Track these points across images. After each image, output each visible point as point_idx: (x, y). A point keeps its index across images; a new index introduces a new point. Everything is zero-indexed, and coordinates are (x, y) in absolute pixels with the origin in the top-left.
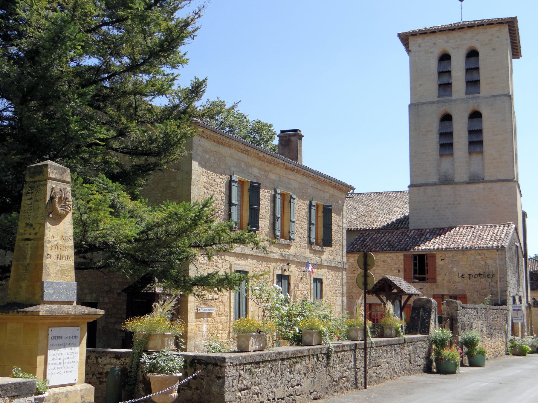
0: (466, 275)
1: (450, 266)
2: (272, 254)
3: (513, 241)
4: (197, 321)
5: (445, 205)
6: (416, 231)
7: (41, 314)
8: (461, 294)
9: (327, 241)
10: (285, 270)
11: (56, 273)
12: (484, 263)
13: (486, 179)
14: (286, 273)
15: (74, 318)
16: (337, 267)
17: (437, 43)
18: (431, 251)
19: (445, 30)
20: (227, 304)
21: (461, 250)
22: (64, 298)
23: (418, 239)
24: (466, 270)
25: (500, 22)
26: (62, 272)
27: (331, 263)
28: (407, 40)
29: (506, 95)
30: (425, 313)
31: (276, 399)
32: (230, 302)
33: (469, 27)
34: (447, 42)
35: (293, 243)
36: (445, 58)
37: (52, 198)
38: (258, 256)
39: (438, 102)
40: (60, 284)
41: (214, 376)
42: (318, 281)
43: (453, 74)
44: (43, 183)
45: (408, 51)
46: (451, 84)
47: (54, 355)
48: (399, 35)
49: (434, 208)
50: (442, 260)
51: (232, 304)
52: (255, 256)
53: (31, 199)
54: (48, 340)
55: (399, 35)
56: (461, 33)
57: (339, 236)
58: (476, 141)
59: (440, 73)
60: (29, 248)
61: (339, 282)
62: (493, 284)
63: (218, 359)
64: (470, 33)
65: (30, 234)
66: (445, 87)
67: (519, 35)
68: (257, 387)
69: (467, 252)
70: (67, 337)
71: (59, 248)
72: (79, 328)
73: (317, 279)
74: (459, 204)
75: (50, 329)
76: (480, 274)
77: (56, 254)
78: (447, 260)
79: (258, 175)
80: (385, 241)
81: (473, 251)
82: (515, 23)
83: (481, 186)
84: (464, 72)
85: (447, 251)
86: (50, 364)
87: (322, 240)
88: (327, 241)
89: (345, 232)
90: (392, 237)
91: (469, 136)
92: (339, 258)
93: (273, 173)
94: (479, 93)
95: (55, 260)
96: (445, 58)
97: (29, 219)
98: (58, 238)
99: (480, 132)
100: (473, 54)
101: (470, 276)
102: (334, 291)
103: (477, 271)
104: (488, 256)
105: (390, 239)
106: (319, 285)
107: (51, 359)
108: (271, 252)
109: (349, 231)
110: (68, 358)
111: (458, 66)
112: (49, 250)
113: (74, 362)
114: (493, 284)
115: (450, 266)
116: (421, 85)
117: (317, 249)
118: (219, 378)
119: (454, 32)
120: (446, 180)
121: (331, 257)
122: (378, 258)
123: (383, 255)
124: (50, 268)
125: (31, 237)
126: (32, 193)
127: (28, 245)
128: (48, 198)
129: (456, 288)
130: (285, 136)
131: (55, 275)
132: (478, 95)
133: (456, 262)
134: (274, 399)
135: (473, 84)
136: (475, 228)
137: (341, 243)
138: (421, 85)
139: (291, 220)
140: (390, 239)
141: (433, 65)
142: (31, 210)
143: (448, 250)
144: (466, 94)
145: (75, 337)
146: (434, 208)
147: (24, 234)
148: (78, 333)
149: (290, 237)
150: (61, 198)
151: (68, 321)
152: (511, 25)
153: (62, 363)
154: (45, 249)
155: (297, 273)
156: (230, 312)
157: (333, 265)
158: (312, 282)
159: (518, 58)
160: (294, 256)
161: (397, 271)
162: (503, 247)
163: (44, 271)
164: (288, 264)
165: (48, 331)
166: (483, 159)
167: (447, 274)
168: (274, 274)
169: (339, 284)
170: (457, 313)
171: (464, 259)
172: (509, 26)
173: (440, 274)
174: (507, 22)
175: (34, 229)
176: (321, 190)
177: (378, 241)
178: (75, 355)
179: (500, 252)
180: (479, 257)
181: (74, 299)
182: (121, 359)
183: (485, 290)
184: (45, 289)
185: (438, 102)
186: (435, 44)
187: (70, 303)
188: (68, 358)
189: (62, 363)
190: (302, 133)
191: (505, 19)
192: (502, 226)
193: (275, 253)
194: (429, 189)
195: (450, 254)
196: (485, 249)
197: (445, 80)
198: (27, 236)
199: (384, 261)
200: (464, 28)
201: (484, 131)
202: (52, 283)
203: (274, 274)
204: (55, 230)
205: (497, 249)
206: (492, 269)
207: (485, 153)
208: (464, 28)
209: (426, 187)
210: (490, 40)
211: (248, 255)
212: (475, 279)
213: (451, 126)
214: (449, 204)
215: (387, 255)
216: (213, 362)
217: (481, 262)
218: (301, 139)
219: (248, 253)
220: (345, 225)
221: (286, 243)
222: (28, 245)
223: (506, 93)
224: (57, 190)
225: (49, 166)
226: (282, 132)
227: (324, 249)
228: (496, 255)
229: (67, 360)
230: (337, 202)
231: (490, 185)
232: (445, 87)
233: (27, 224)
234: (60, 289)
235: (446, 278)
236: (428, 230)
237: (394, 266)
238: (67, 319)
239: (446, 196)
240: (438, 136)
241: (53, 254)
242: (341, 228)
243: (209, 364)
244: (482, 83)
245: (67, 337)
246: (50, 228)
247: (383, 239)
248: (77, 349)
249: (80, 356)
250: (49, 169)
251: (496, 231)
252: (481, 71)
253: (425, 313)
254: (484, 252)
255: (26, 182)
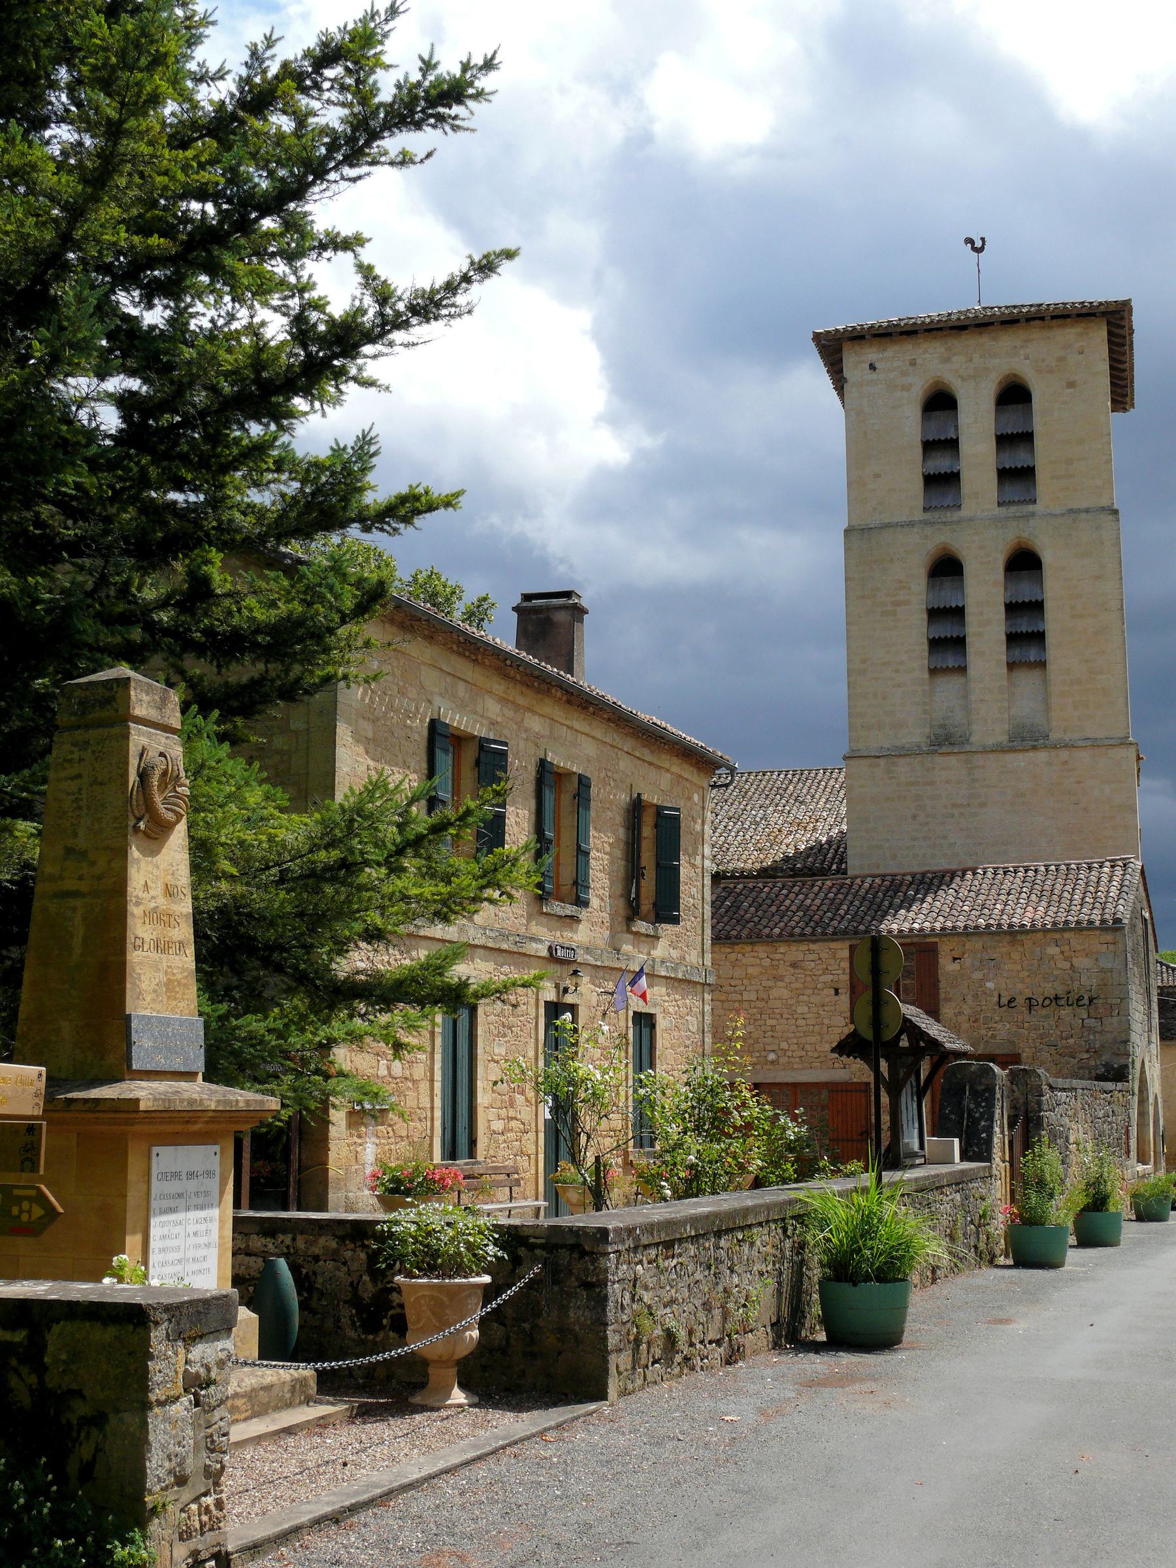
0: (1020, 1000)
1: (977, 975)
2: (534, 945)
3: (1138, 906)
4: (351, 1135)
5: (945, 806)
6: (878, 881)
7: (142, 1107)
8: (1006, 1051)
9: (666, 909)
10: (566, 990)
11: (155, 991)
12: (1067, 965)
13: (1054, 736)
14: (569, 999)
15: (212, 1120)
16: (689, 982)
17: (919, 361)
18: (925, 936)
19: (940, 329)
20: (424, 1086)
21: (1005, 933)
22: (178, 1064)
23: (886, 903)
24: (1020, 986)
25: (1084, 314)
26: (170, 986)
27: (675, 969)
28: (839, 350)
29: (1103, 509)
30: (978, 1105)
31: (706, 1342)
32: (432, 1081)
33: (1004, 323)
34: (947, 360)
35: (584, 914)
36: (940, 402)
37: (143, 776)
38: (499, 950)
39: (926, 523)
40: (167, 1022)
41: (573, 1282)
42: (645, 1022)
43: (965, 447)
44: (116, 730)
45: (839, 383)
46: (958, 474)
47: (163, 1225)
48: (817, 337)
49: (914, 817)
50: (955, 959)
51: (438, 1086)
52: (491, 949)
53: (79, 776)
54: (149, 1182)
55: (817, 337)
56: (984, 340)
57: (695, 892)
58: (1026, 636)
59: (929, 447)
60: (78, 919)
61: (693, 1023)
62: (1091, 1022)
63: (586, 1233)
64: (1007, 341)
65: (81, 878)
66: (942, 484)
67: (1131, 348)
68: (668, 1310)
69: (1023, 937)
70: (191, 1175)
71: (159, 920)
72: (217, 1148)
73: (641, 1014)
74: (982, 805)
75: (155, 1150)
76: (1057, 998)
77: (154, 937)
78: (967, 961)
79: (499, 719)
80: (794, 908)
81: (1040, 935)
82: (1126, 314)
83: (1042, 756)
84: (992, 443)
85: (968, 934)
86: (157, 1251)
87: (654, 905)
88: (666, 909)
89: (708, 881)
90: (812, 896)
91: (1006, 619)
92: (693, 957)
93: (534, 712)
94: (1035, 502)
95: (154, 956)
96: (940, 402)
97: (75, 835)
98: (157, 890)
99: (1037, 607)
100: (1014, 395)
101: (1030, 1003)
102: (682, 1049)
103: (1049, 989)
104: (1079, 948)
105: (808, 902)
106: (646, 1031)
107: (157, 1238)
108: (532, 939)
109: (717, 878)
110: (195, 1234)
111: (977, 424)
112: (139, 929)
113: (208, 1245)
114: (1091, 1022)
115: (977, 975)
116: (877, 476)
117: (643, 931)
118: (588, 1286)
119: (965, 335)
120: (945, 740)
121: (675, 954)
122: (778, 956)
123: (793, 948)
124: (143, 977)
125: (84, 887)
126: (81, 760)
127: (74, 909)
128: (133, 777)
129: (993, 1036)
130: (537, 610)
131: (153, 995)
132: (1031, 508)
133: (993, 963)
134: (702, 1342)
135: (1017, 477)
136: (1036, 871)
137: (698, 913)
138: (877, 476)
139: (579, 846)
140: (808, 902)
141: (910, 424)
142: (80, 808)
143: (971, 933)
144: (999, 504)
145: (209, 1174)
146: (914, 817)
147: (61, 878)
148: (214, 1163)
149: (578, 897)
150: (165, 773)
151: (197, 1127)
152: (1114, 319)
153: (182, 1248)
154: (130, 921)
155: (594, 999)
156: (432, 1108)
157: (680, 976)
158: (630, 1024)
159: (1125, 410)
160: (588, 950)
161: (833, 991)
162: (1117, 921)
163: (128, 986)
164: (575, 973)
165: (149, 1158)
166: (1045, 682)
167: (969, 998)
168: (537, 1000)
169: (694, 1029)
170: (1039, 1103)
171: (1016, 956)
172: (1109, 323)
173: (948, 1000)
174: (1104, 314)
175: (93, 864)
176: (651, 764)
177: (774, 909)
178: (210, 1226)
179: (1109, 937)
180: (1053, 950)
181: (199, 1065)
182: (281, 1237)
183: (1071, 1041)
184: (134, 1037)
185: (926, 523)
186: (913, 363)
187: (189, 1076)
188: (195, 1234)
189: (182, 1248)
190: (584, 603)
191: (1101, 304)
192: (1108, 864)
193: (541, 941)
194: (902, 767)
195: (976, 944)
196: (1071, 929)
197: (941, 463)
198: (69, 885)
199: (794, 965)
200: (992, 324)
201: (1048, 606)
202: (150, 1018)
203: (537, 1000)
204: (150, 868)
205: (1104, 927)
206: (1089, 982)
207: (972, 671)
208: (992, 324)
209: (896, 760)
210: (1061, 359)
211: (476, 946)
212: (1044, 1012)
213: (961, 587)
214: (954, 805)
215: (803, 947)
216: (571, 1240)
217: (1059, 965)
218: (581, 621)
219: (476, 942)
220: (707, 863)
221: (569, 913)
222: (74, 909)
223: (1104, 502)
224: (152, 755)
225: (133, 684)
226: (527, 597)
227: (660, 930)
228: (1096, 942)
229: (192, 1240)
230: (690, 798)
231: (1064, 754)
232: (942, 484)
233: (69, 851)
234: (168, 1037)
235: (967, 1010)
236: (909, 878)
237: (822, 979)
238: (196, 1122)
239: (947, 782)
240: (925, 616)
241: (147, 936)
242: (699, 871)
243: (557, 1247)
244: (1041, 475)
245: (191, 1175)
246: (138, 861)
247: (788, 902)
248: (215, 1213)
249: (221, 1228)
250: (132, 693)
251: (1094, 879)
252: (1038, 442)
253: (978, 1105)
254: (1067, 935)
255: (57, 727)
